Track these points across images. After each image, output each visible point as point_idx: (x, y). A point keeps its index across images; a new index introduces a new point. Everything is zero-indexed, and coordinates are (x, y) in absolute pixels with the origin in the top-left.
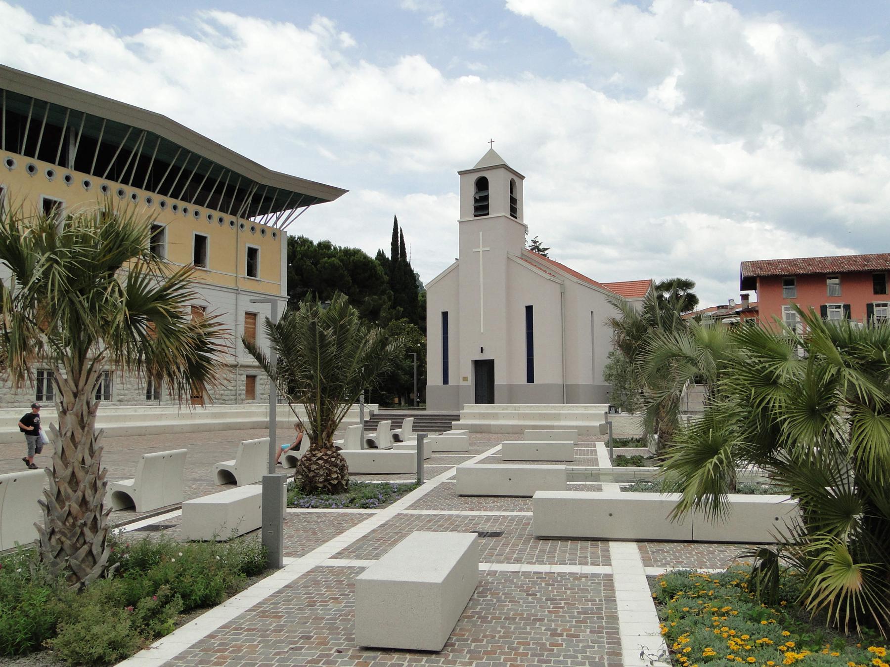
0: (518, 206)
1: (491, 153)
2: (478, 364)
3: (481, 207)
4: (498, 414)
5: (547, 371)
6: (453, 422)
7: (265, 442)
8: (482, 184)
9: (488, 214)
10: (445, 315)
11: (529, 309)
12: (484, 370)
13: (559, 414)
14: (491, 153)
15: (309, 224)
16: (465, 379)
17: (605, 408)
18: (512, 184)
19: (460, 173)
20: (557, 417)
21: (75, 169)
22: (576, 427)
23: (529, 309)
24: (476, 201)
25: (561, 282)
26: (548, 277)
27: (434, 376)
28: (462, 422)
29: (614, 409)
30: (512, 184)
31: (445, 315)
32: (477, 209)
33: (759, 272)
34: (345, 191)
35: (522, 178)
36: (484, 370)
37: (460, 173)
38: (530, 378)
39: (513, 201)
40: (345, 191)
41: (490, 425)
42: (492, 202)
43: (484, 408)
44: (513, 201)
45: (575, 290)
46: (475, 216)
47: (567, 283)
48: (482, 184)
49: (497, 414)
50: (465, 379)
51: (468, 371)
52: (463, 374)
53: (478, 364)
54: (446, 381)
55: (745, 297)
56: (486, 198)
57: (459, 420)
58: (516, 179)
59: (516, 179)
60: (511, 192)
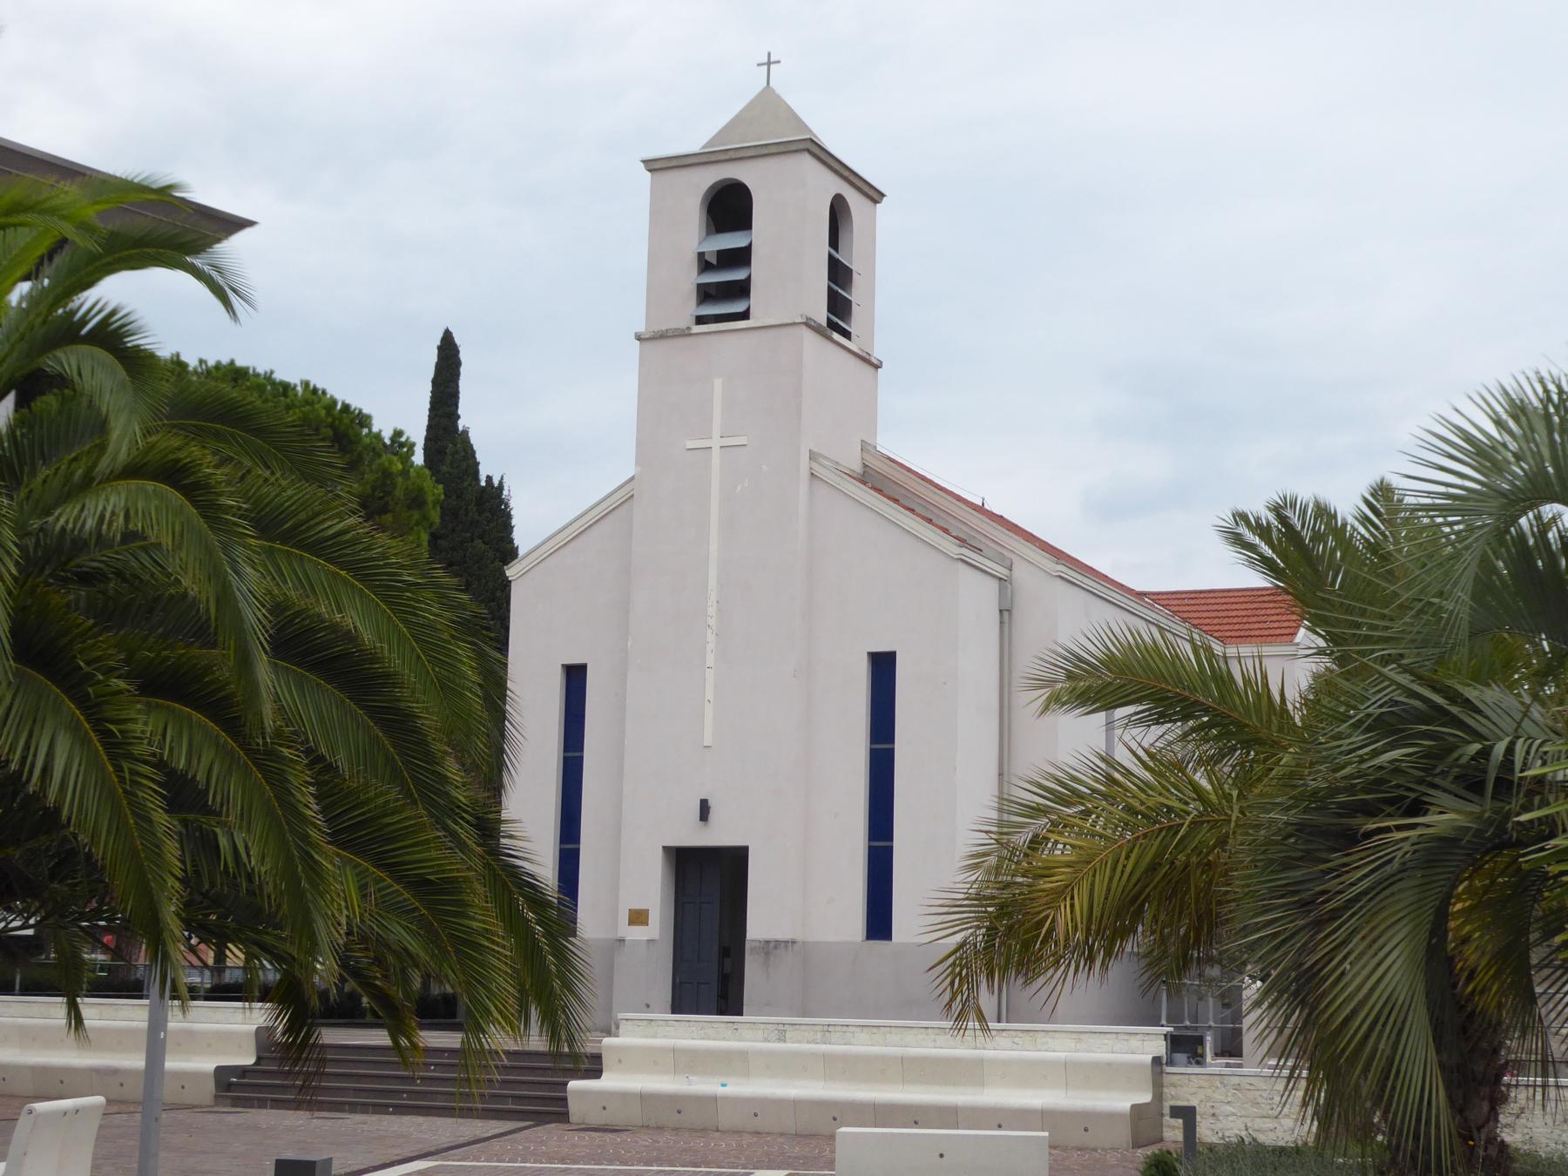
0: (856, 295)
1: (768, 102)
3: (724, 288)
4: (745, 1063)
6: (574, 1084)
7: (92, 1108)
8: (729, 207)
9: (745, 315)
10: (575, 677)
11: (883, 667)
12: (710, 883)
14: (768, 102)
16: (638, 918)
17: (1149, 1043)
18: (838, 214)
20: (973, 1072)
21: (677, 1008)
22: (1045, 1117)
23: (883, 667)
24: (705, 265)
25: (1001, 571)
26: (953, 549)
28: (610, 1081)
29: (1185, 1046)
30: (838, 214)
31: (575, 677)
32: (706, 294)
34: (251, 223)
35: (874, 195)
36: (710, 883)
39: (839, 273)
40: (251, 223)
41: (714, 1099)
42: (760, 272)
43: (704, 1033)
44: (839, 273)
45: (1031, 576)
46: (700, 320)
47: (1021, 573)
48: (729, 207)
49: (743, 1055)
50: (638, 918)
51: (649, 887)
52: (622, 906)
56: (741, 257)
57: (596, 1073)
58: (853, 199)
59: (853, 199)
60: (834, 242)
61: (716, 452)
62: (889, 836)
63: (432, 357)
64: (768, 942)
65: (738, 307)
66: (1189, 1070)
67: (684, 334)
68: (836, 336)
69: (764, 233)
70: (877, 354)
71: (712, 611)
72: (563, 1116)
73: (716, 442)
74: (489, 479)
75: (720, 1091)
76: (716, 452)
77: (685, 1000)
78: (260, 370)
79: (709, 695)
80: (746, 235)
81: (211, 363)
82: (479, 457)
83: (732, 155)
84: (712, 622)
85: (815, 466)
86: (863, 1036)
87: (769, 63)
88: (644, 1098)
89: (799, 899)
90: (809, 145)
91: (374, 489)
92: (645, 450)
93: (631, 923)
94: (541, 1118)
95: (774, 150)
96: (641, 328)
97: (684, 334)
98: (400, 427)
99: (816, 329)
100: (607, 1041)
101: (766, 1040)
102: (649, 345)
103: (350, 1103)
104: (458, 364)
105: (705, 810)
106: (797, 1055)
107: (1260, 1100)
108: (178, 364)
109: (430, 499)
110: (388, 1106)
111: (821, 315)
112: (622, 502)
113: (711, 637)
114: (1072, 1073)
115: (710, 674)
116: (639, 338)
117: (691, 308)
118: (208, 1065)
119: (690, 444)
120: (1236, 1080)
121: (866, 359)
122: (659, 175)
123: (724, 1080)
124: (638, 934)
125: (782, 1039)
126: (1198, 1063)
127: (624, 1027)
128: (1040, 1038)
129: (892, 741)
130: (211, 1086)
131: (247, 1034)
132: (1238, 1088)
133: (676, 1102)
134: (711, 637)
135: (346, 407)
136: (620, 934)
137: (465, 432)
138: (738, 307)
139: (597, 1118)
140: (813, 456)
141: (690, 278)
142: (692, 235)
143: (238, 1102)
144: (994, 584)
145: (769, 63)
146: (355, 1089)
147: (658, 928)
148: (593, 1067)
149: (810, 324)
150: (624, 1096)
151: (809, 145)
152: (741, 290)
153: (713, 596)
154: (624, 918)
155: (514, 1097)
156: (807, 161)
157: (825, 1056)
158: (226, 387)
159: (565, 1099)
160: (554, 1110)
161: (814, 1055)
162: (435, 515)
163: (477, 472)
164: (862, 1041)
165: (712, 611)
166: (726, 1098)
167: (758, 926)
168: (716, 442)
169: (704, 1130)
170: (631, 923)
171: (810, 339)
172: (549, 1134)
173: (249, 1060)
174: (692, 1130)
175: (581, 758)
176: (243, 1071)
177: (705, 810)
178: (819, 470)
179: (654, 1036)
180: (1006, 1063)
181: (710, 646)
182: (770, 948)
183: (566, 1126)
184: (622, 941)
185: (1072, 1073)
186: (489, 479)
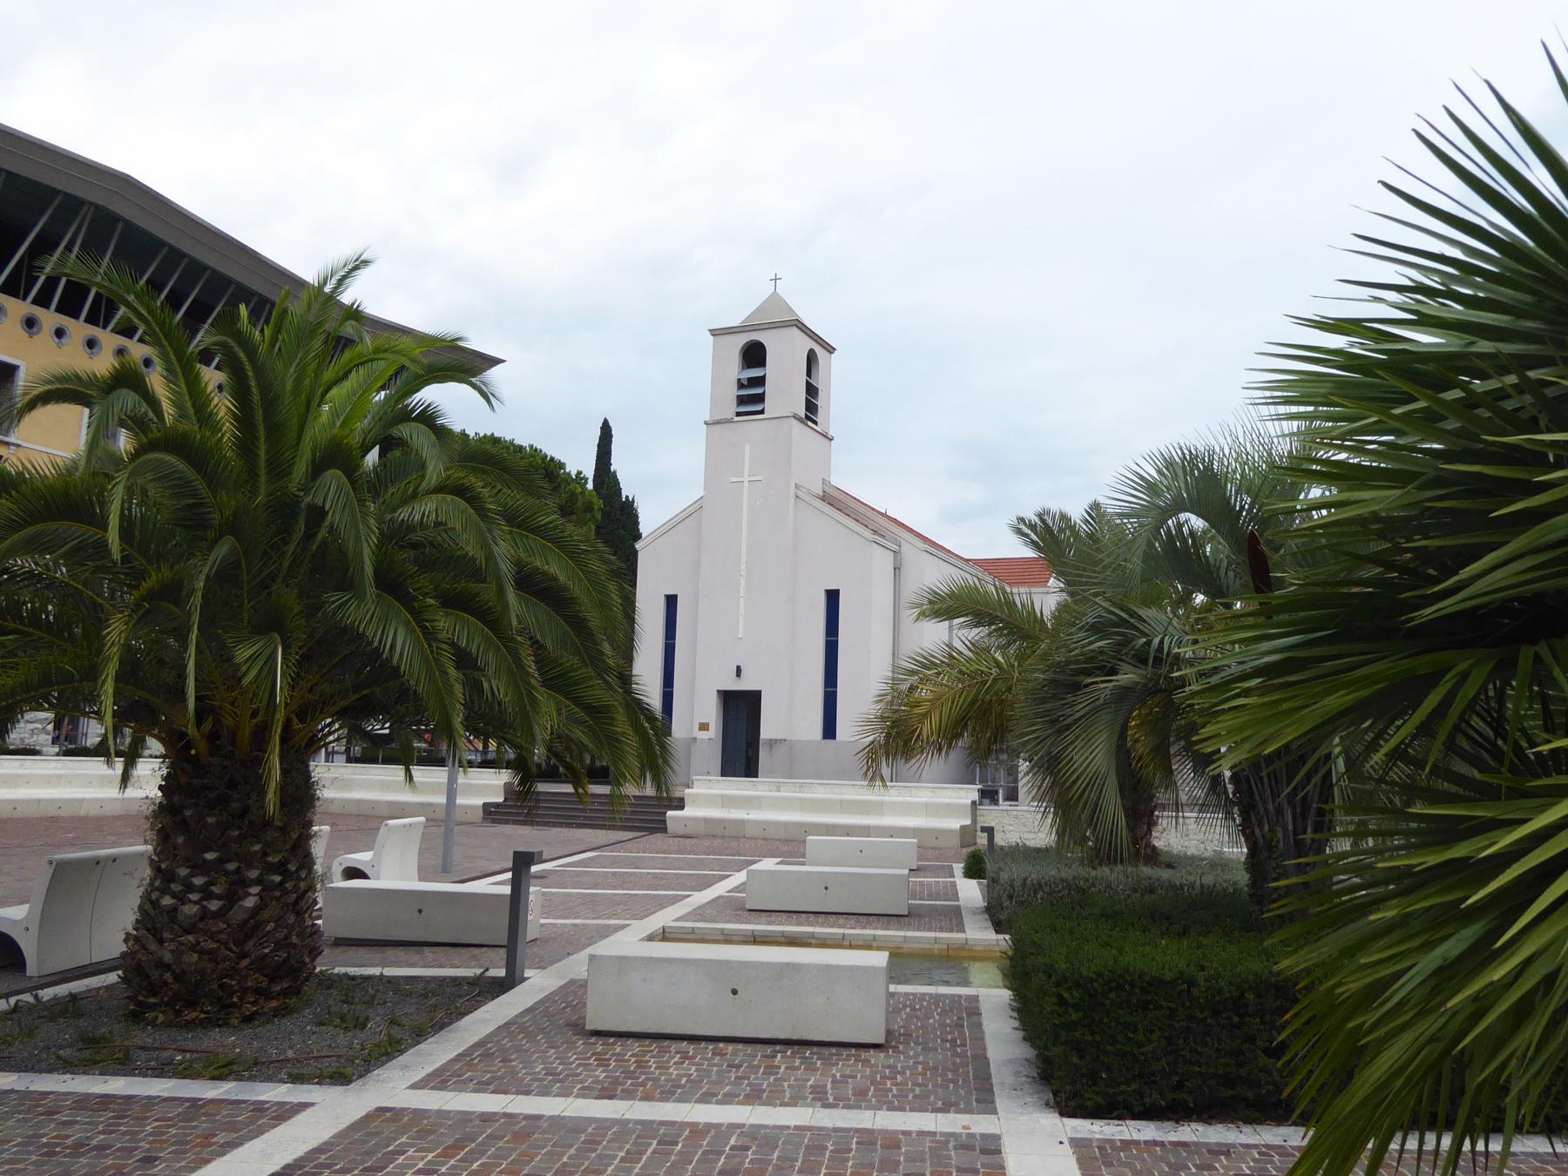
1: (775, 299)
3: (751, 397)
6: (670, 813)
8: (754, 355)
9: (762, 412)
10: (671, 601)
11: (833, 597)
12: (741, 708)
14: (775, 299)
16: (704, 727)
19: (715, 333)
21: (723, 775)
23: (833, 597)
25: (895, 548)
28: (688, 812)
31: (671, 601)
32: (741, 400)
35: (830, 350)
36: (741, 708)
37: (715, 333)
39: (812, 390)
41: (742, 822)
43: (738, 787)
46: (738, 414)
48: (754, 355)
50: (704, 727)
51: (710, 711)
56: (761, 381)
57: (682, 808)
65: (759, 408)
69: (771, 370)
72: (664, 830)
73: (746, 479)
75: (745, 817)
77: (727, 770)
88: (706, 820)
89: (788, 717)
92: (708, 484)
94: (652, 831)
105: (739, 671)
106: (786, 799)
111: (802, 413)
117: (734, 408)
118: (479, 802)
121: (825, 436)
140: (797, 486)
141: (733, 392)
142: (734, 369)
143: (494, 821)
147: (714, 732)
148: (680, 804)
149: (796, 417)
150: (695, 819)
152: (760, 398)
153: (744, 560)
160: (660, 827)
162: (599, 516)
164: (820, 791)
167: (766, 732)
173: (501, 800)
176: (497, 805)
177: (739, 671)
178: (800, 494)
182: (772, 743)
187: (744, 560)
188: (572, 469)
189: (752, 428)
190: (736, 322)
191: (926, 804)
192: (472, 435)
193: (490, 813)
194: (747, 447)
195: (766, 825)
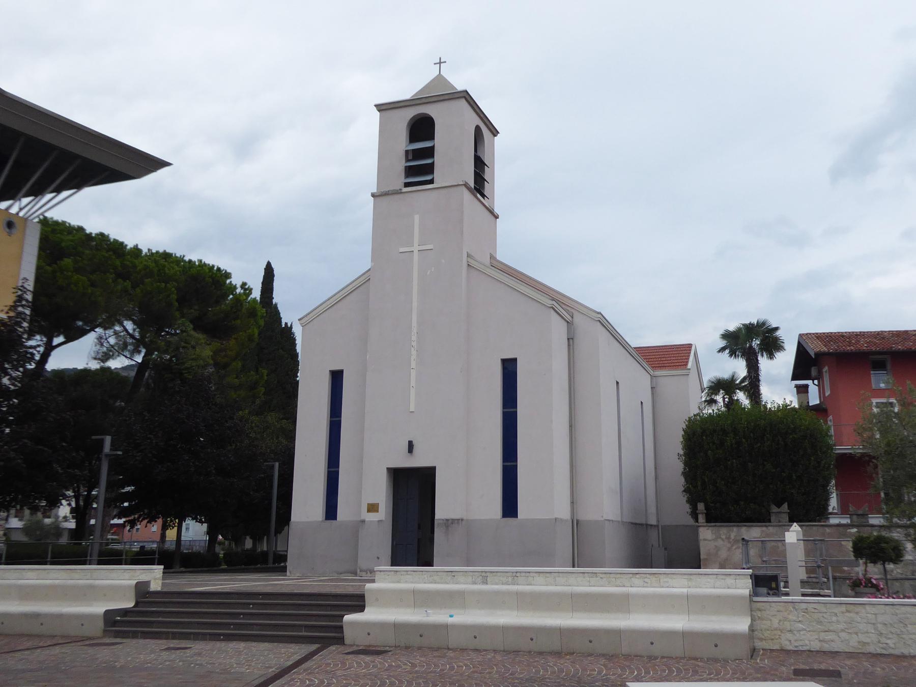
1: (440, 79)
2: (504, 362)
3: (419, 166)
5: (545, 495)
6: (348, 618)
8: (422, 128)
9: (431, 182)
10: (337, 377)
11: (509, 368)
12: (414, 489)
13: (627, 597)
14: (440, 79)
15: (89, 209)
16: (373, 508)
19: (381, 108)
20: (622, 604)
21: (393, 564)
23: (509, 368)
25: (568, 317)
26: (549, 302)
27: (307, 502)
28: (370, 615)
31: (337, 377)
32: (410, 171)
33: (833, 348)
35: (495, 132)
36: (414, 489)
37: (381, 108)
38: (510, 507)
39: (480, 164)
41: (446, 627)
43: (412, 579)
46: (407, 185)
48: (422, 128)
49: (461, 594)
50: (373, 508)
51: (378, 491)
53: (504, 362)
54: (331, 511)
55: (802, 390)
56: (429, 152)
57: (361, 608)
61: (416, 253)
62: (515, 459)
63: (262, 273)
64: (447, 520)
65: (429, 178)
66: (770, 599)
67: (398, 192)
68: (478, 195)
69: (441, 140)
70: (497, 210)
71: (414, 338)
72: (340, 641)
73: (416, 248)
74: (286, 324)
75: (450, 620)
76: (416, 253)
77: (398, 559)
78: (178, 255)
79: (413, 383)
80: (429, 142)
81: (154, 251)
82: (282, 315)
83: (424, 101)
84: (414, 344)
85: (469, 260)
86: (540, 579)
87: (440, 63)
88: (397, 627)
89: (465, 497)
90: (465, 94)
91: (232, 308)
92: (377, 252)
93: (369, 511)
94: (326, 643)
95: (446, 97)
96: (375, 190)
97: (398, 192)
98: (245, 281)
99: (469, 188)
100: (369, 586)
101: (474, 583)
102: (378, 199)
103: (194, 634)
104: (273, 276)
105: (411, 447)
106: (497, 593)
107: (822, 619)
108: (136, 251)
109: (259, 314)
110: (220, 635)
111: (472, 184)
112: (363, 283)
113: (414, 352)
114: (694, 604)
115: (413, 373)
116: (373, 195)
117: (402, 180)
118: (99, 609)
119: (402, 250)
120: (804, 606)
121: (491, 212)
122: (384, 113)
123: (452, 612)
124: (372, 517)
125: (485, 582)
126: (775, 595)
127: (378, 576)
128: (663, 579)
129: (516, 407)
130: (101, 624)
131: (129, 586)
132: (806, 611)
133: (419, 629)
134: (414, 352)
135: (219, 269)
136: (362, 518)
137: (276, 305)
138: (429, 178)
139: (363, 641)
140: (469, 256)
141: (401, 164)
142: (401, 143)
143: (118, 634)
144: (566, 324)
145: (440, 63)
146: (198, 623)
147: (384, 513)
148: (358, 603)
149: (466, 185)
150: (383, 625)
151: (465, 94)
152: (430, 169)
153: (415, 330)
154: (364, 508)
155: (306, 626)
156: (463, 102)
157: (518, 594)
158: (162, 262)
159: (341, 627)
160: (333, 635)
161: (509, 593)
162: (262, 323)
163: (281, 322)
164: (539, 583)
165: (414, 338)
166: (454, 626)
167: (441, 513)
168: (416, 248)
169: (438, 649)
170: (369, 511)
171: (467, 195)
172: (332, 654)
173: (130, 604)
174: (431, 649)
175: (340, 421)
176: (125, 612)
177: (411, 447)
178: (473, 263)
179: (399, 582)
180: (645, 597)
181: (414, 357)
182: (449, 523)
183: (341, 648)
184: (363, 521)
185: (694, 604)
186: (286, 324)
187: (415, 330)
188: (236, 280)
189: (422, 198)
190: (407, 96)
191: (688, 597)
192: (145, 251)
193: (115, 623)
194: (417, 218)
195: (477, 630)
